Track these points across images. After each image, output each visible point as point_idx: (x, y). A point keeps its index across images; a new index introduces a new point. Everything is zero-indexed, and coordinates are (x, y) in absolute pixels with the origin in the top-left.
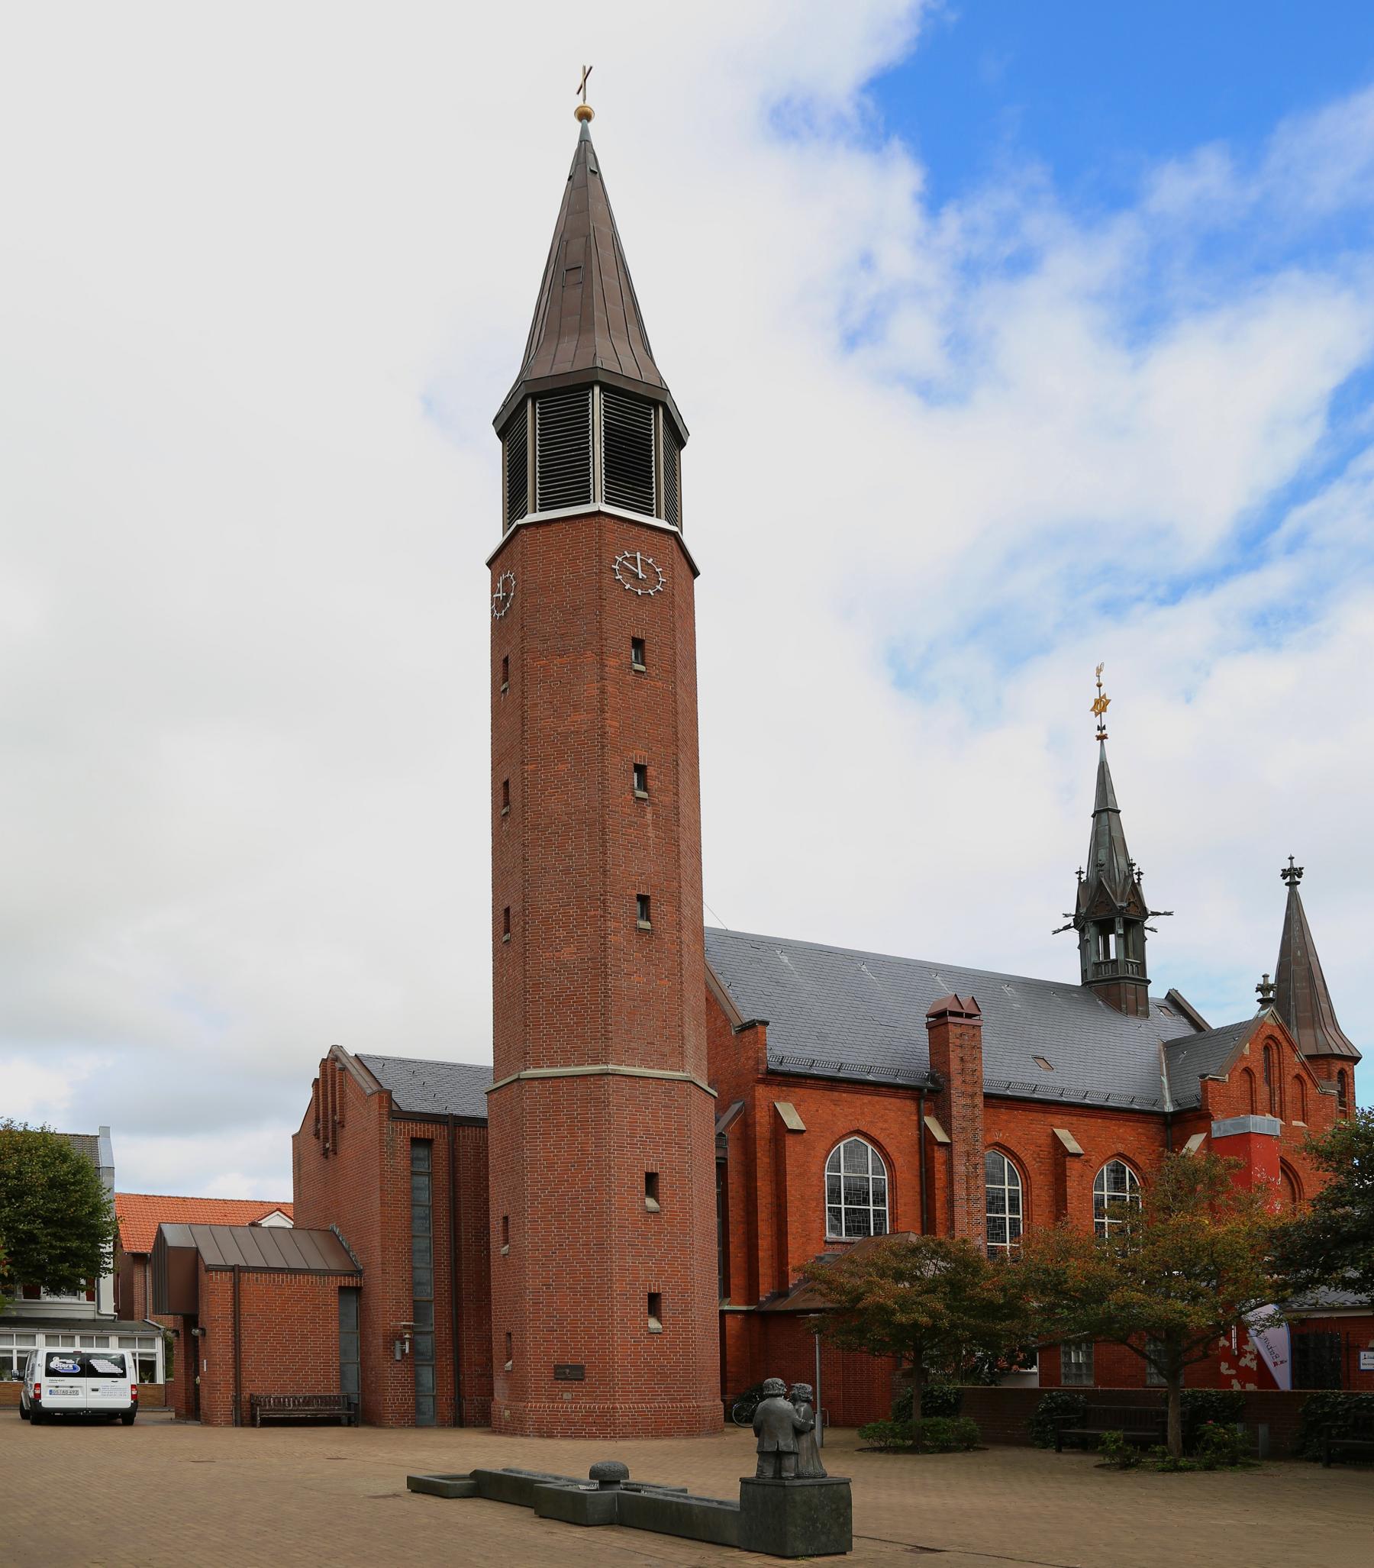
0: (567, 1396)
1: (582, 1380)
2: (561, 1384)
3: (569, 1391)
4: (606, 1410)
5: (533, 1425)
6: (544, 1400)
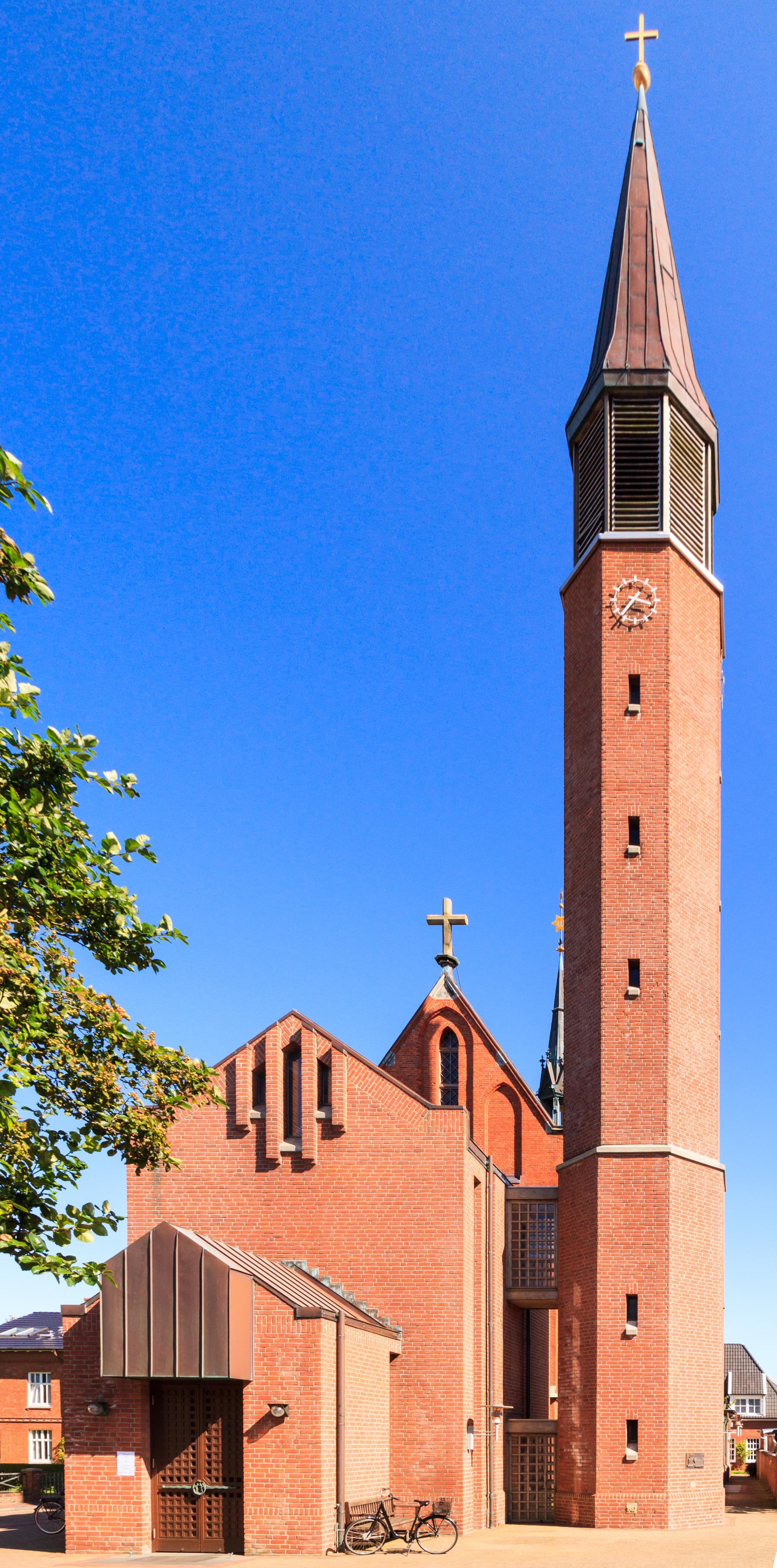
0: (693, 1484)
1: (702, 1467)
2: (689, 1472)
3: (693, 1480)
4: (613, 1499)
5: (674, 1516)
6: (678, 1489)
